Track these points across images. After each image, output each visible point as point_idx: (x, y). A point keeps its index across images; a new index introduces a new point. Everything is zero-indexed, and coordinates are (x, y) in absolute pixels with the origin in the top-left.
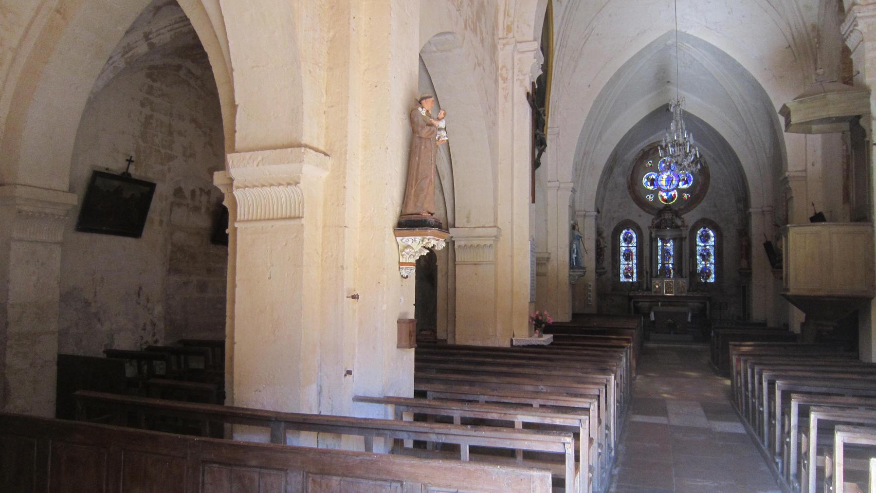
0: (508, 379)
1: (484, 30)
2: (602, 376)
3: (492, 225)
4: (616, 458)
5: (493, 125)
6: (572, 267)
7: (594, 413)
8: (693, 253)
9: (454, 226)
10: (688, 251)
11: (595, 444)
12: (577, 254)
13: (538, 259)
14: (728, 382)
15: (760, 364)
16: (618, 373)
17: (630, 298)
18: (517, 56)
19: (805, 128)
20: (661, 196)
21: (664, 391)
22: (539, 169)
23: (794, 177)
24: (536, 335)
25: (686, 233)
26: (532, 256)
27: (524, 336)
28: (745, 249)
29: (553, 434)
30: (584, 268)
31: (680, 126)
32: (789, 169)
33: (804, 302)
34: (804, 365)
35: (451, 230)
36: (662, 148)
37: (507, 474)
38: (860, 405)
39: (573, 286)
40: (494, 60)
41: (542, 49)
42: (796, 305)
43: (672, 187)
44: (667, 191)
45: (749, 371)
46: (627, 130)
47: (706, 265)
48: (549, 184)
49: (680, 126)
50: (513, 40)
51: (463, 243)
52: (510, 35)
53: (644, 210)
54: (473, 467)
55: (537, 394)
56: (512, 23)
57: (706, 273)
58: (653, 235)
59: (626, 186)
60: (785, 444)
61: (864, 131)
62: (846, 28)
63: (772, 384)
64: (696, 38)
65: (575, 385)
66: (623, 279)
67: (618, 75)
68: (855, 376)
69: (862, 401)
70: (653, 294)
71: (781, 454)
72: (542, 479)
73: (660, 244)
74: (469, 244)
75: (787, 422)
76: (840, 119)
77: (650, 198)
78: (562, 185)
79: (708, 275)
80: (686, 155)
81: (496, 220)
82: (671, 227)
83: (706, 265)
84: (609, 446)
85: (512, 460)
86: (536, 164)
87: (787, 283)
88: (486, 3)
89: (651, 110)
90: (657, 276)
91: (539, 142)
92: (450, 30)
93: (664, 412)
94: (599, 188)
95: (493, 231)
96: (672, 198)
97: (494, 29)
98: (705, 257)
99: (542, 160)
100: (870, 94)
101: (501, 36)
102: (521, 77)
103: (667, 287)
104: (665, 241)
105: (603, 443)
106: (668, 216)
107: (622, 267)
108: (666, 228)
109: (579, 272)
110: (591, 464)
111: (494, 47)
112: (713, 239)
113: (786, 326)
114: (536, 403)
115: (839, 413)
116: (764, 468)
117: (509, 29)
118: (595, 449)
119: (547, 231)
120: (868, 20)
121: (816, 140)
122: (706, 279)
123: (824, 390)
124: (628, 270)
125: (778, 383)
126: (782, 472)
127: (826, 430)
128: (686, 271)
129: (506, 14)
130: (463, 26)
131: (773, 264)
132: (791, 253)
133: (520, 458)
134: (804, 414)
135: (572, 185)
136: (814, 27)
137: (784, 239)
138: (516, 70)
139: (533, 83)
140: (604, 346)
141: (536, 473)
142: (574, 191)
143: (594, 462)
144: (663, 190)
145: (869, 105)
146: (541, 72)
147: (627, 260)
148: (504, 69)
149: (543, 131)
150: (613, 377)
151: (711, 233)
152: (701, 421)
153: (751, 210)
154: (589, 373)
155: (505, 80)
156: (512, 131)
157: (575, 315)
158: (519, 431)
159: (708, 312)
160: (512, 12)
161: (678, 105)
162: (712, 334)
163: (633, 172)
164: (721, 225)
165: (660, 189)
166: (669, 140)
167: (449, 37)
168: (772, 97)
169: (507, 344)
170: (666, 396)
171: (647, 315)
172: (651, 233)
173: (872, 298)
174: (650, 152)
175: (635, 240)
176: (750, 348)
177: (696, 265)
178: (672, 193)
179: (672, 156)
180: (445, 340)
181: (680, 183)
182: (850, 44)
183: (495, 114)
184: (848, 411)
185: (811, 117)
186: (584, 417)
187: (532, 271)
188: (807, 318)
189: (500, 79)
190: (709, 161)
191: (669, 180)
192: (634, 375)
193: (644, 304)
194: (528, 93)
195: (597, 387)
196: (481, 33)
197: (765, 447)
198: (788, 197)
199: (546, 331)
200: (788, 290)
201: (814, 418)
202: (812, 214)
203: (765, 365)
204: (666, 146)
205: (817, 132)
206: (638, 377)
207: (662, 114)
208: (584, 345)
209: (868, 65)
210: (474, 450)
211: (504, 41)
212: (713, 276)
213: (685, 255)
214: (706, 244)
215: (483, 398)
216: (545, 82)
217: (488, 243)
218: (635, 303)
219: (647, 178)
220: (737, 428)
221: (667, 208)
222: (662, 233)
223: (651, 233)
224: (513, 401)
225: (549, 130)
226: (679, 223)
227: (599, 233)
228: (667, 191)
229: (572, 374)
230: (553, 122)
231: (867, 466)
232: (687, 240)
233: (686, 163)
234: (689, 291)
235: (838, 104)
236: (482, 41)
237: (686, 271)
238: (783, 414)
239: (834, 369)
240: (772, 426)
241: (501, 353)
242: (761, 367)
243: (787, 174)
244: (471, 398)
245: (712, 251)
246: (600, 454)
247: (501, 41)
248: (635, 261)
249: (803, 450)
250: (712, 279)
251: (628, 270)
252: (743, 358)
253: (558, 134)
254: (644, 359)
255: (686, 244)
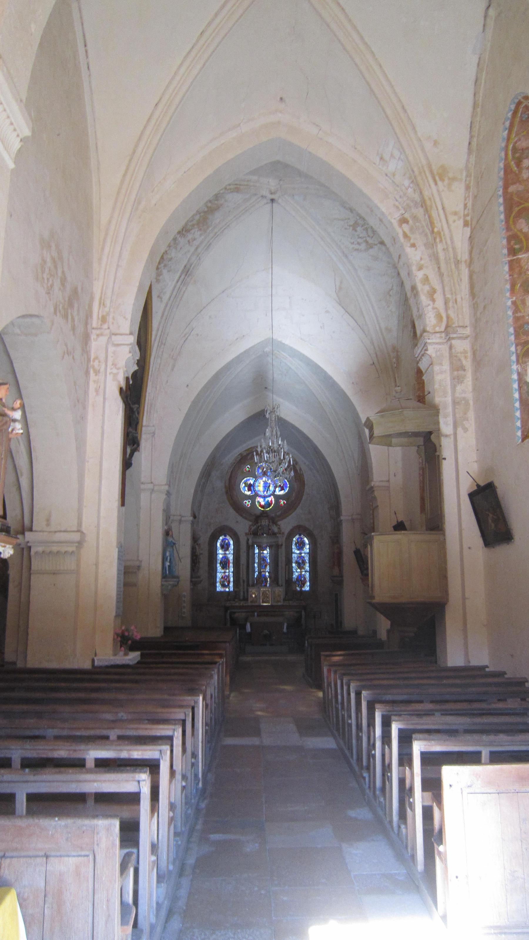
0: (85, 707)
1: (76, 319)
2: (189, 698)
3: (75, 529)
4: (204, 790)
5: (81, 420)
6: (164, 576)
7: (177, 742)
8: (289, 561)
9: (31, 530)
10: (284, 558)
11: (178, 777)
12: (170, 562)
13: (126, 568)
14: (321, 694)
15: (348, 674)
16: (208, 693)
17: (226, 609)
18: (111, 349)
19: (386, 440)
20: (259, 502)
21: (258, 708)
22: (131, 469)
23: (379, 487)
24: (122, 653)
25: (282, 540)
26: (119, 564)
27: (108, 655)
28: (337, 558)
29: (127, 772)
30: (178, 577)
31: (274, 433)
32: (375, 480)
33: (389, 610)
34: (388, 673)
35: (27, 534)
36: (257, 454)
37: (66, 826)
38: (437, 711)
39: (165, 597)
40: (85, 351)
41: (139, 343)
42: (382, 613)
43: (269, 493)
44: (264, 497)
45: (339, 682)
46: (224, 434)
47: (301, 572)
48: (142, 486)
49: (274, 433)
50: (108, 331)
51: (40, 549)
52: (105, 326)
53: (241, 516)
54: (30, 821)
55: (114, 723)
56: (108, 314)
57: (301, 581)
58: (250, 542)
59: (224, 490)
60: (371, 756)
61: (435, 445)
62: (419, 351)
63: (358, 694)
64: (291, 348)
65: (159, 710)
66: (219, 588)
67: (217, 377)
68: (433, 682)
69: (438, 707)
70: (250, 604)
71: (368, 768)
72: (108, 829)
73: (257, 551)
74: (48, 550)
75: (372, 734)
76: (416, 434)
77: (248, 503)
78: (156, 488)
79: (303, 584)
80: (280, 462)
81: (80, 524)
82: (268, 534)
83: (301, 572)
84: (196, 776)
85: (80, 806)
86: (127, 463)
87: (372, 590)
88: (79, 290)
89: (250, 415)
90: (253, 585)
91: (131, 440)
92: (36, 313)
93: (257, 732)
94: (196, 491)
95: (76, 537)
96: (269, 504)
97: (87, 318)
98: (301, 565)
99: (134, 460)
100: (439, 412)
101: (94, 325)
102: (115, 371)
103: (264, 596)
104: (261, 548)
105: (189, 775)
106: (265, 522)
107: (219, 575)
108: (263, 534)
109: (172, 582)
110: (173, 800)
111: (86, 339)
112: (308, 547)
113: (375, 632)
114: (113, 734)
115: (415, 720)
116: (354, 784)
117: (104, 320)
118: (179, 782)
119: (139, 538)
120: (436, 346)
121: (397, 452)
122: (301, 587)
123: (405, 697)
124: (224, 579)
125: (364, 693)
126: (369, 787)
127: (406, 739)
128: (282, 580)
129: (102, 303)
130: (52, 310)
131: (362, 572)
132: (376, 564)
133: (91, 802)
134: (386, 724)
135: (166, 487)
136: (394, 349)
137: (369, 547)
138: (110, 363)
139: (127, 379)
140: (194, 663)
141: (101, 823)
142: (168, 494)
143: (177, 796)
144: (260, 496)
145: (438, 423)
146: (136, 368)
147: (223, 568)
148: (97, 361)
149: (136, 429)
150: (201, 698)
151: (306, 541)
152: (294, 738)
153: (342, 518)
154: (174, 695)
155: (97, 372)
156: (103, 428)
157: (167, 629)
158: (90, 771)
159: (303, 621)
160: (108, 303)
161: (273, 411)
162: (306, 645)
163: (231, 477)
164: (315, 532)
165: (257, 495)
166: (263, 446)
167: (34, 320)
168: (359, 409)
169: (87, 665)
170: (259, 713)
171: (243, 627)
172: (248, 540)
173: (446, 604)
174: (246, 458)
175: (232, 547)
176: (341, 658)
177: (292, 573)
178: (269, 499)
179: (266, 462)
180: (14, 663)
181: (277, 489)
182: (423, 366)
183: (84, 408)
184: (425, 718)
185: (391, 431)
186: (166, 748)
187: (119, 580)
188: (392, 625)
189: (92, 371)
190: (304, 467)
191: (266, 486)
192: (227, 693)
193: (240, 615)
194: (121, 389)
195: (182, 710)
196: (73, 320)
197: (354, 762)
198: (374, 506)
199: (132, 648)
200: (373, 597)
201: (395, 728)
202: (394, 523)
203: (352, 675)
204: (262, 451)
205: (397, 445)
206: (232, 695)
207: (258, 420)
208: (172, 663)
209: (436, 386)
210: (32, 798)
211: (98, 332)
212: (308, 584)
213: (282, 562)
214: (301, 551)
215: (51, 732)
216: (142, 379)
217: (70, 549)
218: (231, 613)
219: (245, 483)
220: (328, 743)
221: (264, 514)
222: (258, 540)
223: (248, 540)
224: (92, 733)
225: (144, 429)
226: (276, 529)
227: (195, 539)
228: (264, 497)
229: (157, 696)
230: (149, 420)
231: (440, 773)
232: (284, 547)
233: (281, 470)
234: (284, 600)
235: (413, 421)
236: (73, 329)
237: (282, 580)
238: (369, 726)
239: (413, 675)
240: (359, 739)
241: (79, 676)
242: (349, 677)
243: (373, 484)
244: (37, 733)
245: (307, 559)
246: (184, 788)
247: (94, 331)
248: (232, 569)
249: (387, 762)
250: (307, 588)
251: (224, 579)
252: (333, 669)
253: (154, 433)
254: (239, 674)
255: (282, 551)
